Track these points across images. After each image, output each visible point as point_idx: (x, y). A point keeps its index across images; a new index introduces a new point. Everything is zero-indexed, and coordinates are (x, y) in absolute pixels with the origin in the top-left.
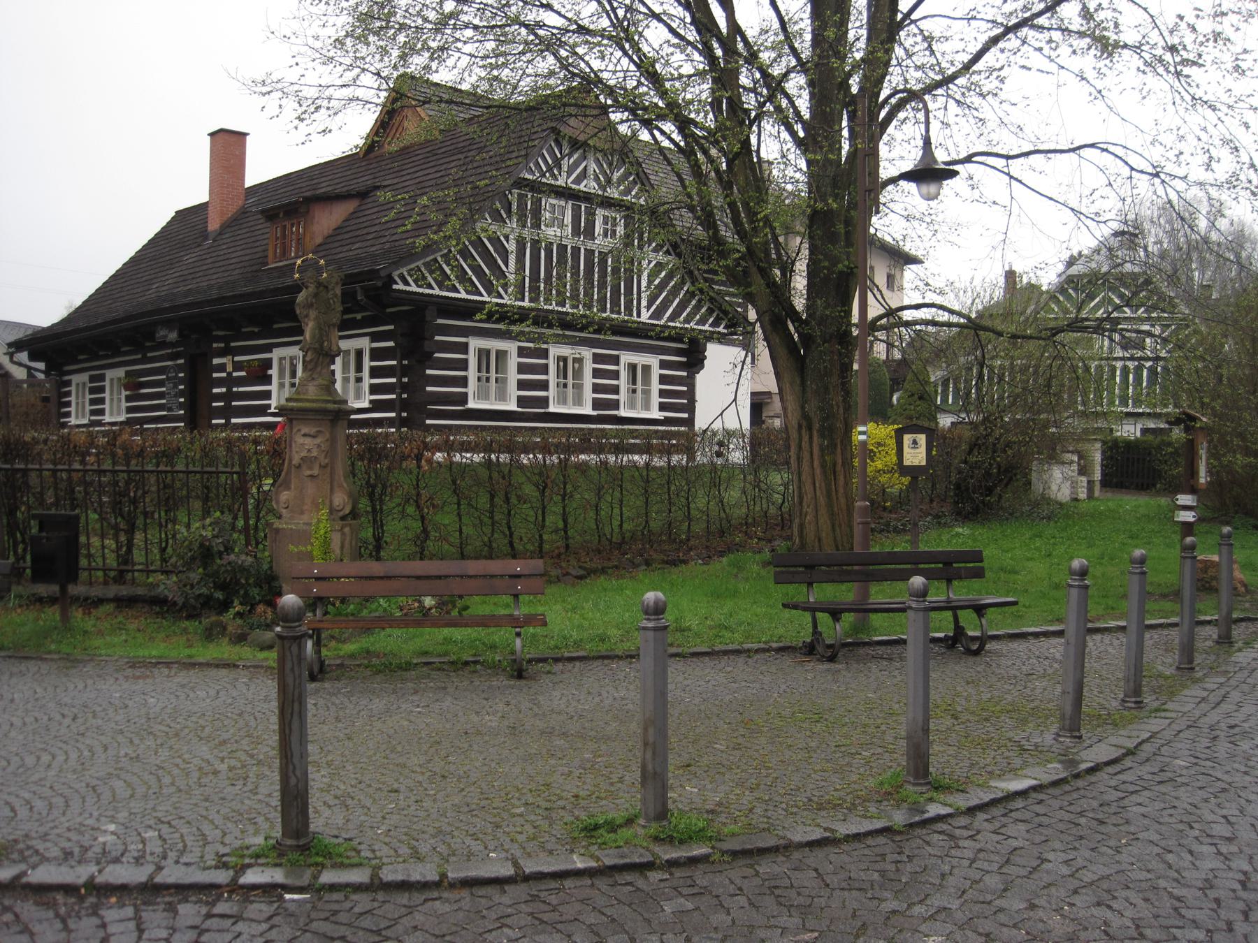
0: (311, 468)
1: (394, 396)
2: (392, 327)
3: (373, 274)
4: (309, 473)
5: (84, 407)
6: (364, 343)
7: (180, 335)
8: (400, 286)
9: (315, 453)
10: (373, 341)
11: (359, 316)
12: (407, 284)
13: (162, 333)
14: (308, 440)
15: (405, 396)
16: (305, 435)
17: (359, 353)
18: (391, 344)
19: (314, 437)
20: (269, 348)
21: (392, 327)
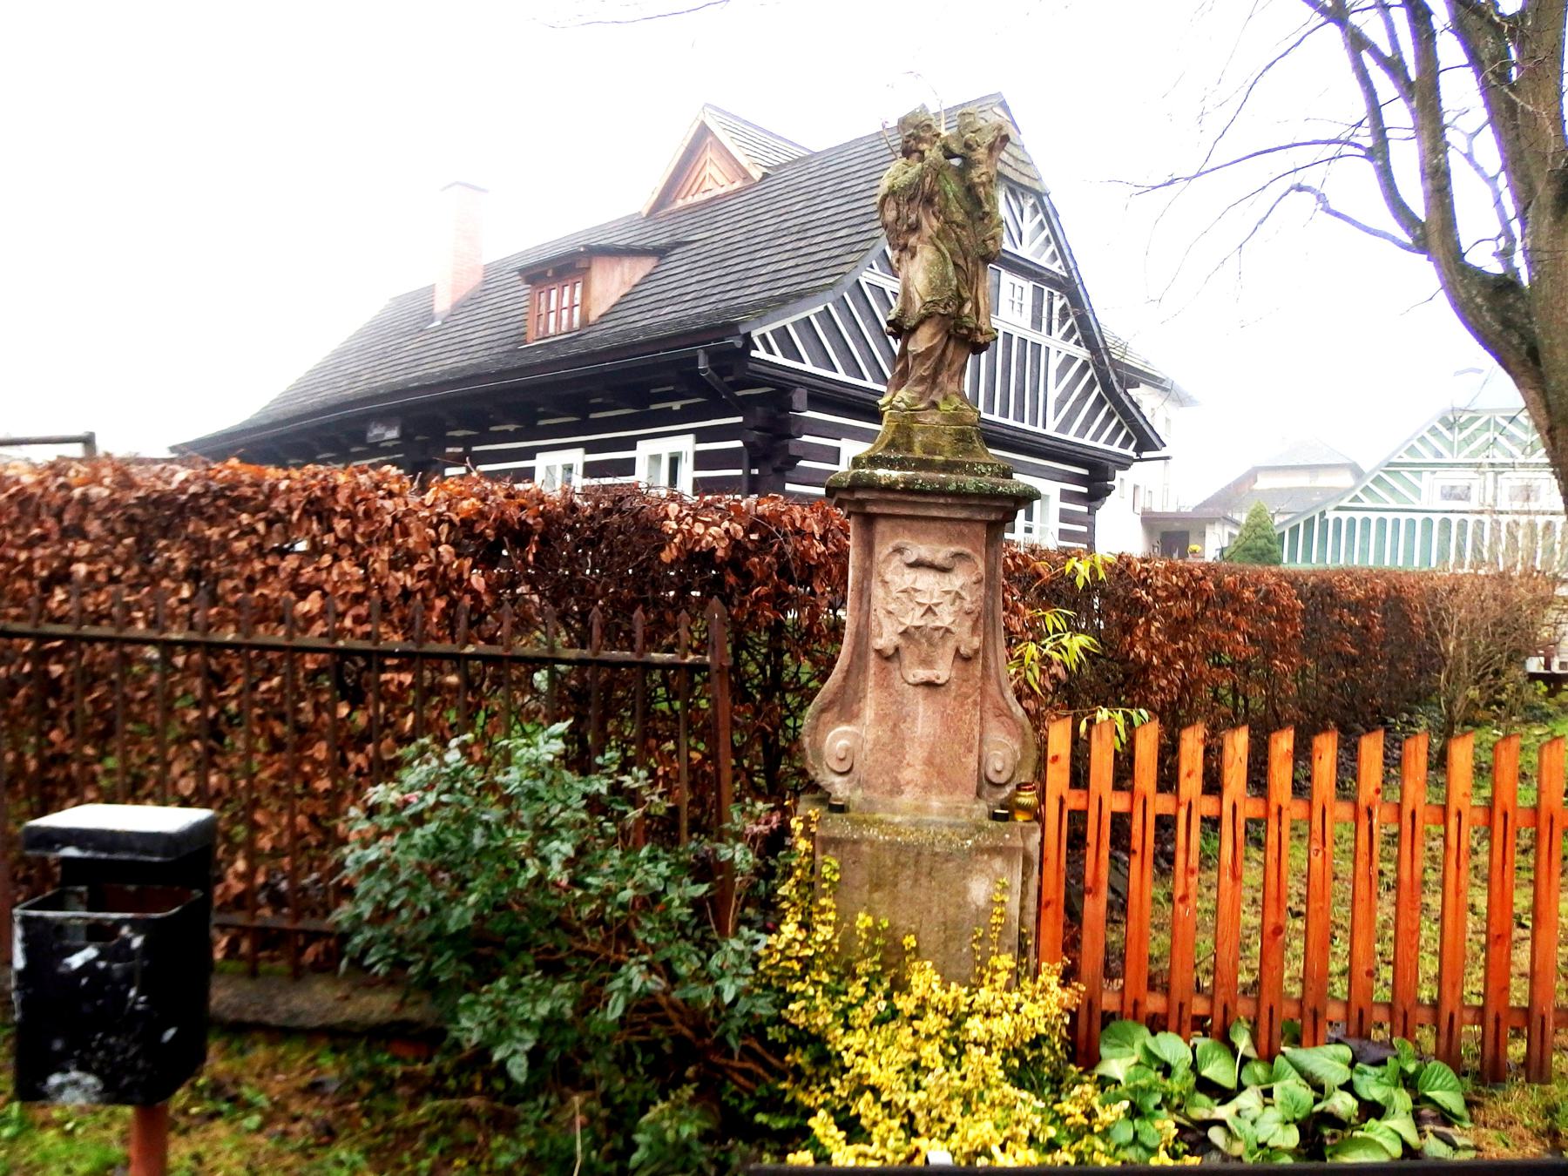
0: (927, 662)
2: (739, 419)
3: (731, 328)
4: (922, 674)
6: (686, 445)
7: (404, 435)
9: (945, 618)
10: (698, 441)
11: (676, 406)
12: (770, 351)
13: (376, 431)
14: (926, 580)
16: (917, 565)
17: (674, 461)
18: (738, 444)
19: (943, 570)
20: (530, 454)
21: (739, 419)
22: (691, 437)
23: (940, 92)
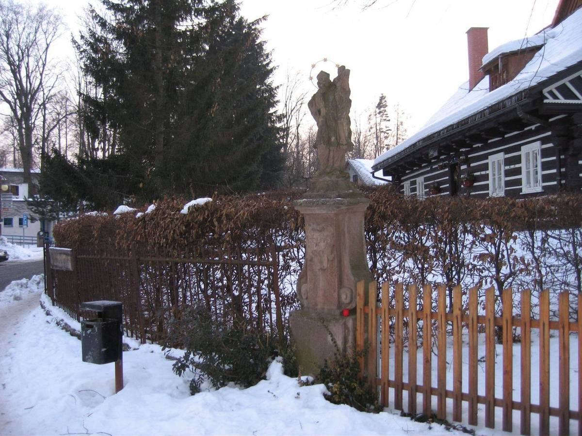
1: (555, 183)
2: (549, 133)
5: (500, 179)
8: (550, 100)
10: (543, 144)
11: (533, 127)
12: (556, 97)
15: (563, 182)
20: (485, 157)
21: (549, 133)
22: (538, 143)
23: (32, 224)
